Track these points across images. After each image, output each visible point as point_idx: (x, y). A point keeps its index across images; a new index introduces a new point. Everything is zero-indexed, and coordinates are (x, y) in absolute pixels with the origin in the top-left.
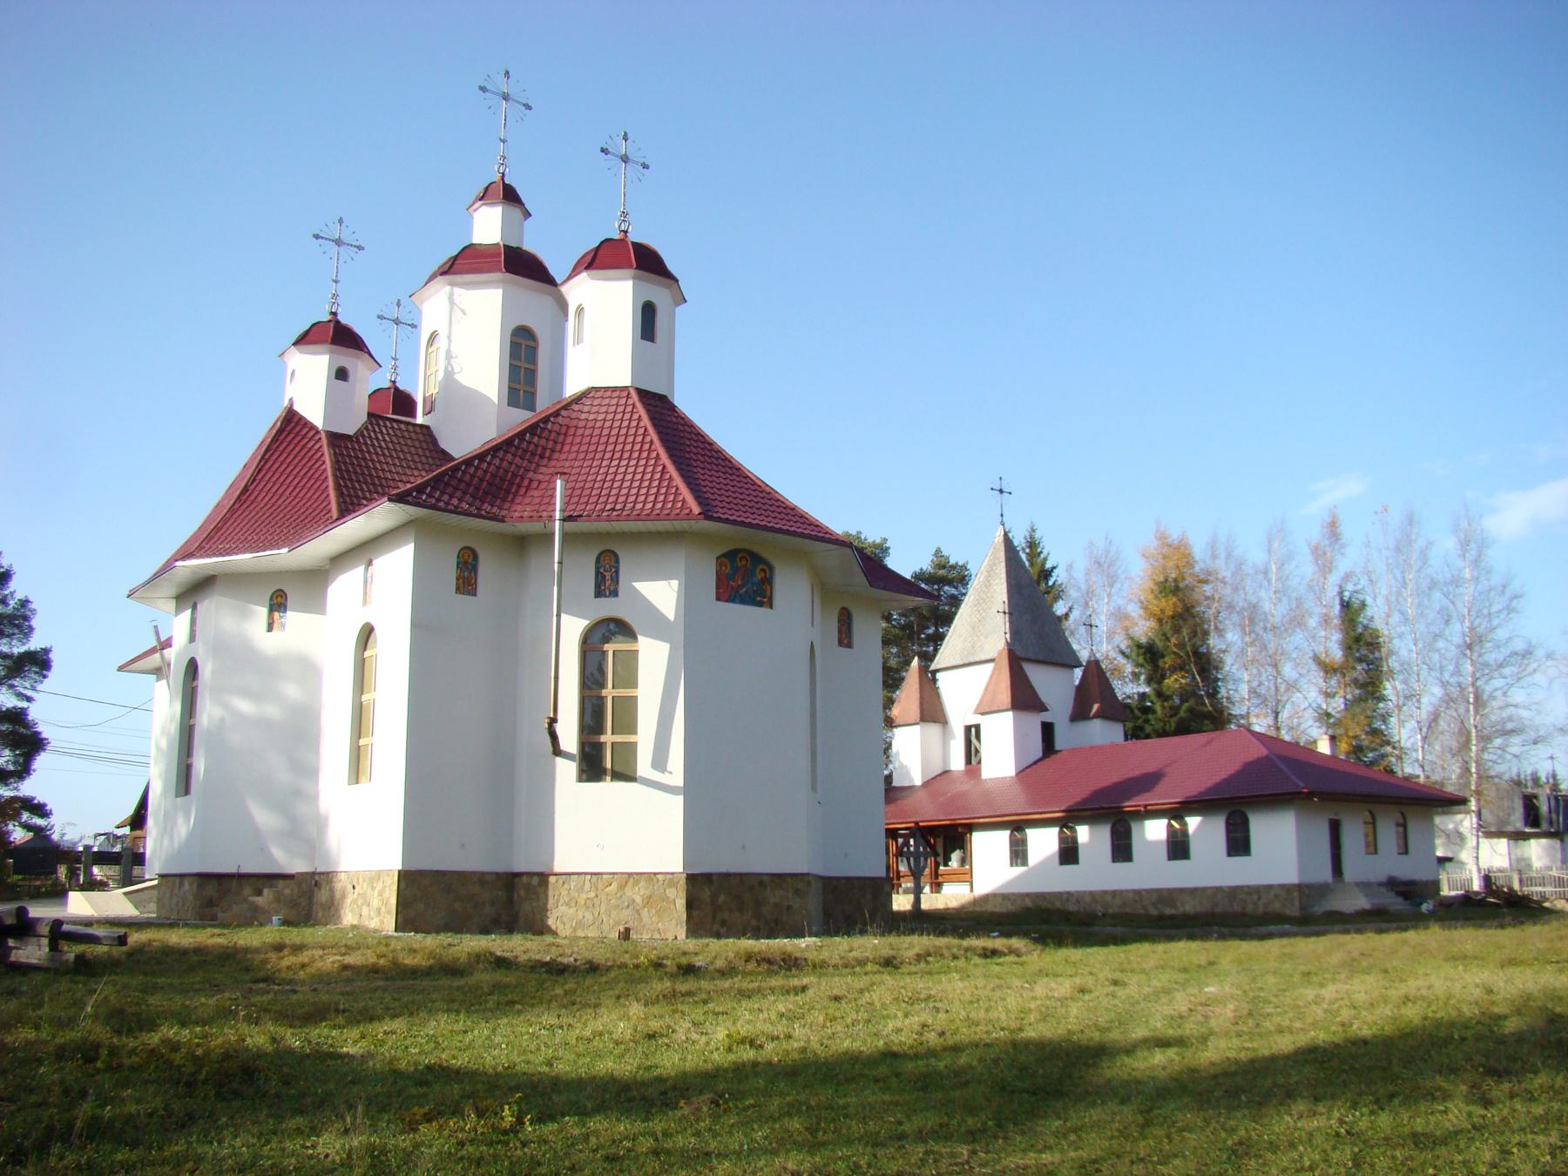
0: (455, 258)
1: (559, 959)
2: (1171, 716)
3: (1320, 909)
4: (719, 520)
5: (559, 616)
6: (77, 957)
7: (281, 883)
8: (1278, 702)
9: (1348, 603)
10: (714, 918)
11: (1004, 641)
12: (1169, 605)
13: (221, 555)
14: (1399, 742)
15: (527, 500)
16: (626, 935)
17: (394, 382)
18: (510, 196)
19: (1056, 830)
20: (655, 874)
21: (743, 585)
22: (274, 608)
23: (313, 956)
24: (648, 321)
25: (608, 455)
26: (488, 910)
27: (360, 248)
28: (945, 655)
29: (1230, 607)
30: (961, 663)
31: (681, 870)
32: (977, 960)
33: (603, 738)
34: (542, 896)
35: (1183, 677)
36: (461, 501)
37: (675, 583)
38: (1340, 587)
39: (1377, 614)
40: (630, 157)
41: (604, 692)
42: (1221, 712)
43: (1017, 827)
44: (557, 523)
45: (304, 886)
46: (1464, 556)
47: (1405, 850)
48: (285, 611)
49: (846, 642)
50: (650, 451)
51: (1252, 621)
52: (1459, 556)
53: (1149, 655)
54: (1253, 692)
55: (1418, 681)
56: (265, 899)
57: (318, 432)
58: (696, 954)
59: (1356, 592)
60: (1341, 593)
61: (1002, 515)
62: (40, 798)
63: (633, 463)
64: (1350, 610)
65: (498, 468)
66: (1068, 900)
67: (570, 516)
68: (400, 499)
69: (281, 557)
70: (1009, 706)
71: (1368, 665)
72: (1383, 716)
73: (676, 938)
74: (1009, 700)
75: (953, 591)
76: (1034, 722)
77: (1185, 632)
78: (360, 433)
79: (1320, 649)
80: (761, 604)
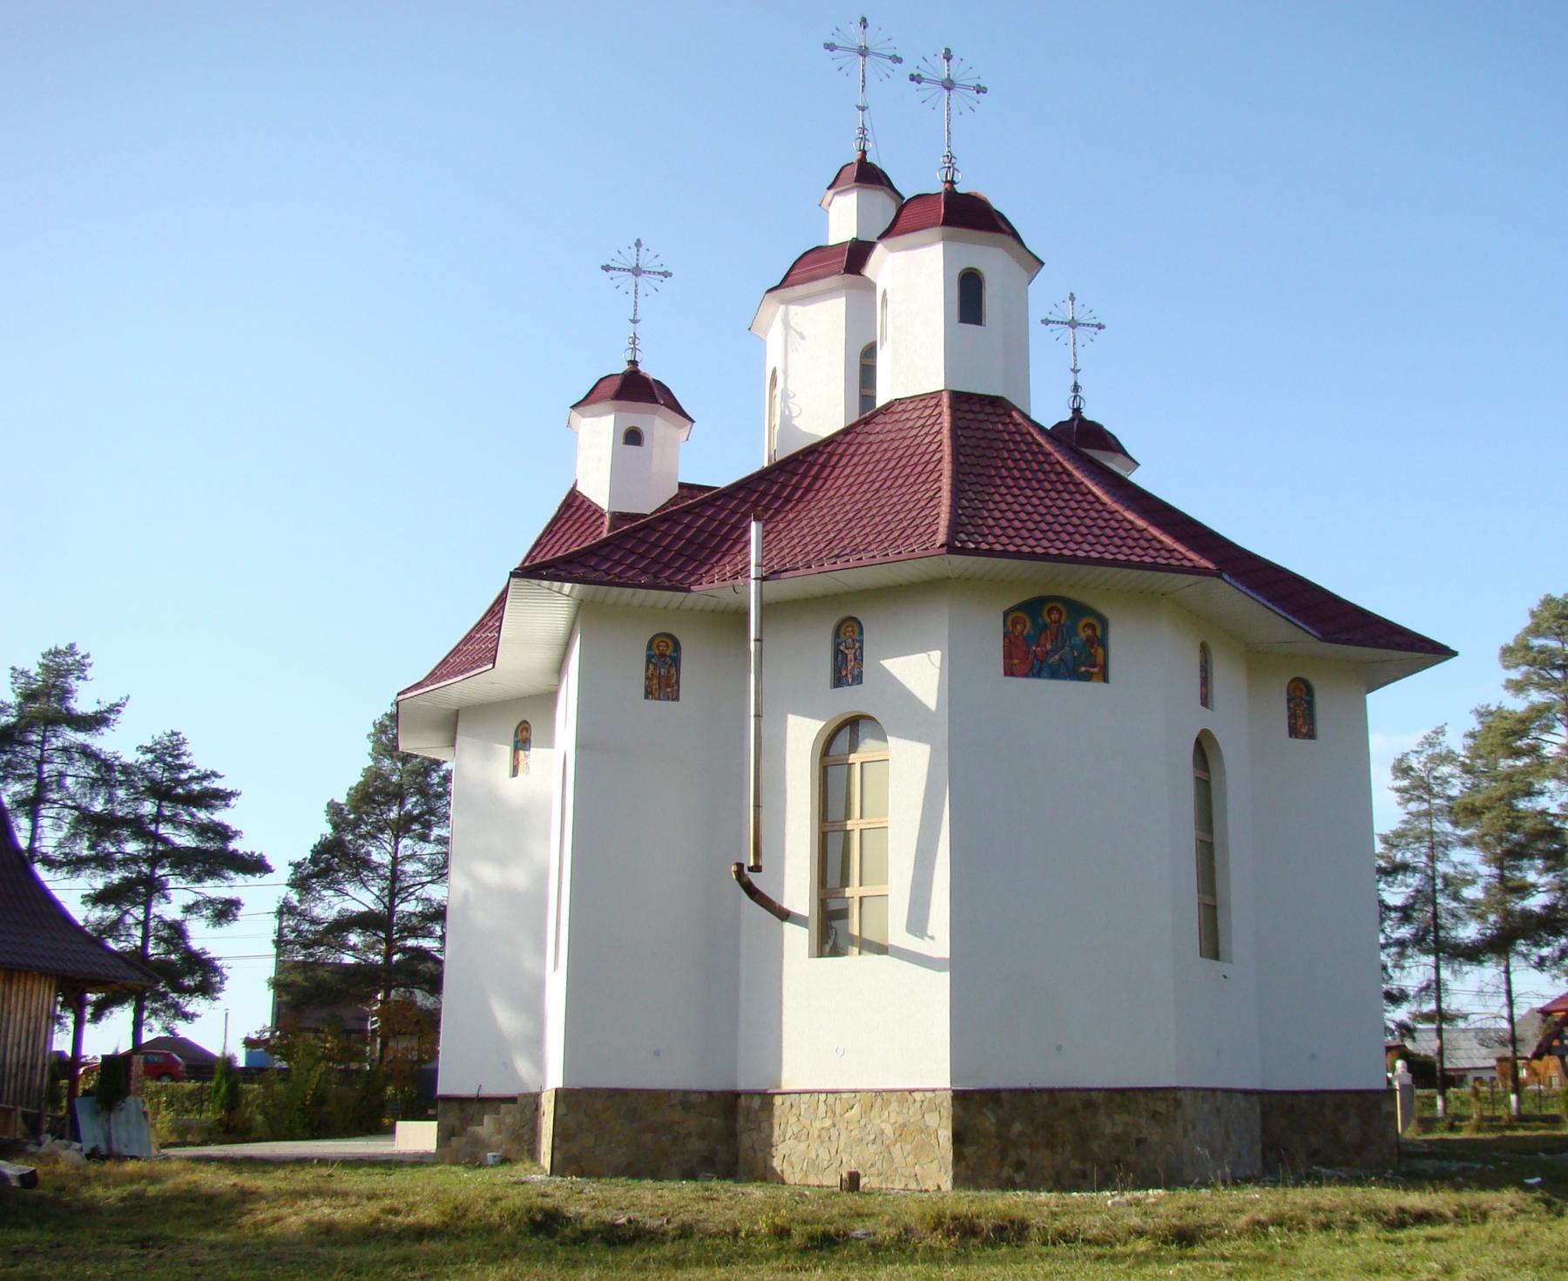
10: (1003, 1159)
16: (853, 1182)
20: (911, 1091)
21: (1054, 651)
22: (520, 745)
26: (696, 1145)
27: (666, 274)
31: (948, 1086)
34: (765, 1125)
37: (936, 655)
44: (753, 583)
48: (529, 750)
49: (1304, 730)
57: (602, 515)
73: (939, 1188)
80: (1087, 677)
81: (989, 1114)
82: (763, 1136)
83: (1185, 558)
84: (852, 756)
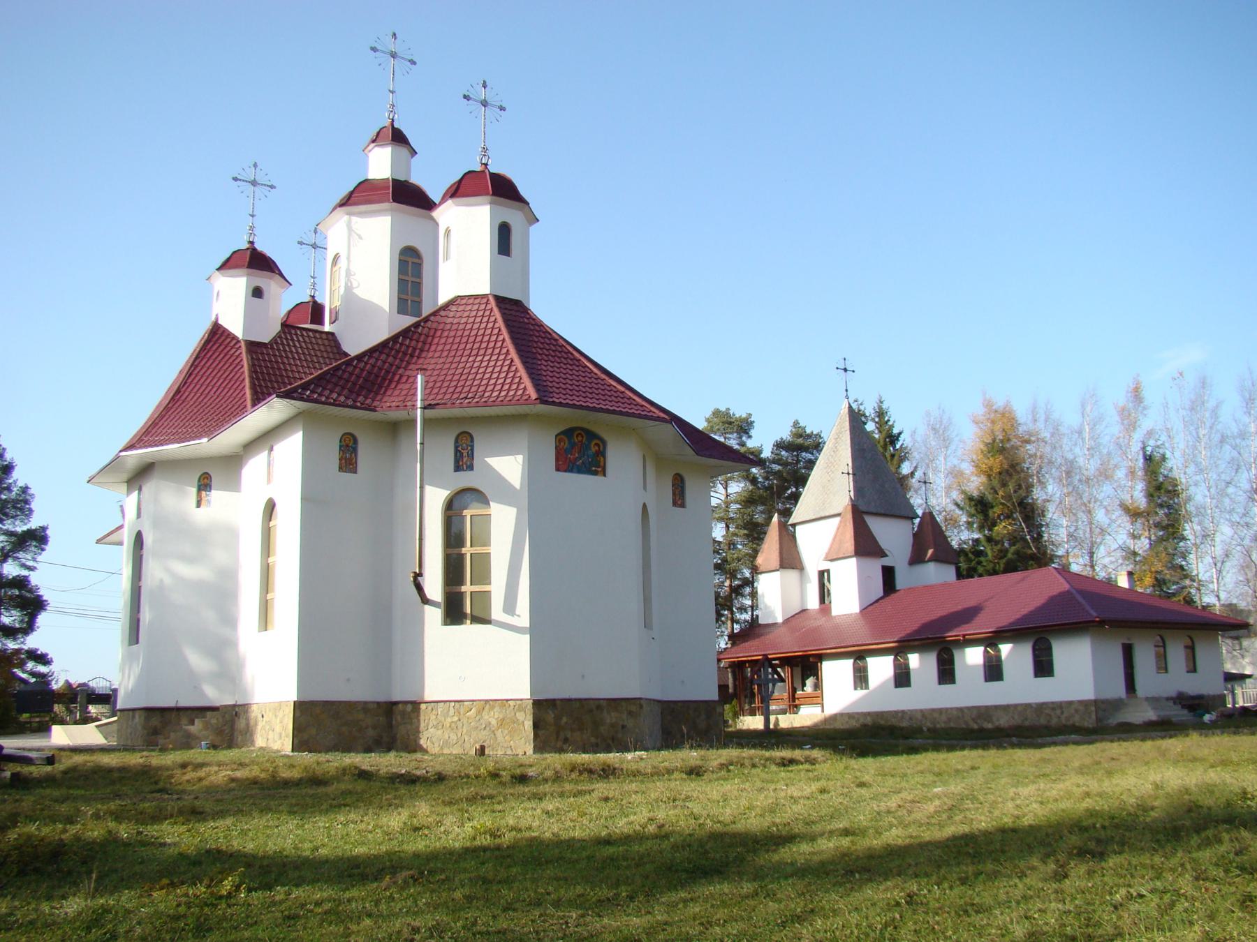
0: (352, 193)
1: (414, 772)
2: (1001, 558)
3: (1113, 721)
4: (553, 403)
5: (422, 487)
6: (13, 775)
7: (209, 714)
8: (1093, 543)
9: (1150, 456)
10: (557, 737)
11: (848, 498)
12: (997, 462)
13: (156, 446)
14: (1197, 575)
15: (397, 392)
17: (313, 297)
18: (399, 138)
19: (891, 658)
20: (507, 700)
23: (210, 771)
24: (504, 239)
25: (467, 353)
26: (371, 733)
27: (272, 187)
28: (799, 514)
29: (1050, 462)
30: (814, 517)
32: (774, 768)
33: (463, 589)
35: (1010, 524)
36: (339, 395)
37: (520, 458)
38: (1143, 443)
39: (1175, 465)
40: (489, 101)
41: (464, 550)
42: (1045, 553)
43: (860, 656)
44: (419, 410)
45: (227, 716)
46: (1249, 413)
47: (1193, 669)
48: (210, 491)
50: (501, 347)
51: (1068, 473)
52: (1245, 413)
53: (979, 507)
54: (1070, 535)
55: (1212, 522)
56: (197, 727)
57: (238, 341)
58: (531, 766)
59: (1158, 447)
60: (1144, 449)
61: (847, 390)
62: (42, 649)
63: (494, 358)
64: (1152, 463)
65: (374, 366)
66: (902, 717)
67: (430, 405)
68: (287, 395)
69: (203, 446)
70: (853, 553)
71: (1169, 509)
72: (1183, 553)
74: (853, 548)
75: (809, 456)
76: (875, 566)
77: (1011, 487)
78: (274, 340)
79: (1126, 498)
80: (595, 473)
81: (551, 712)
82: (414, 727)
83: (651, 411)
84: (465, 511)
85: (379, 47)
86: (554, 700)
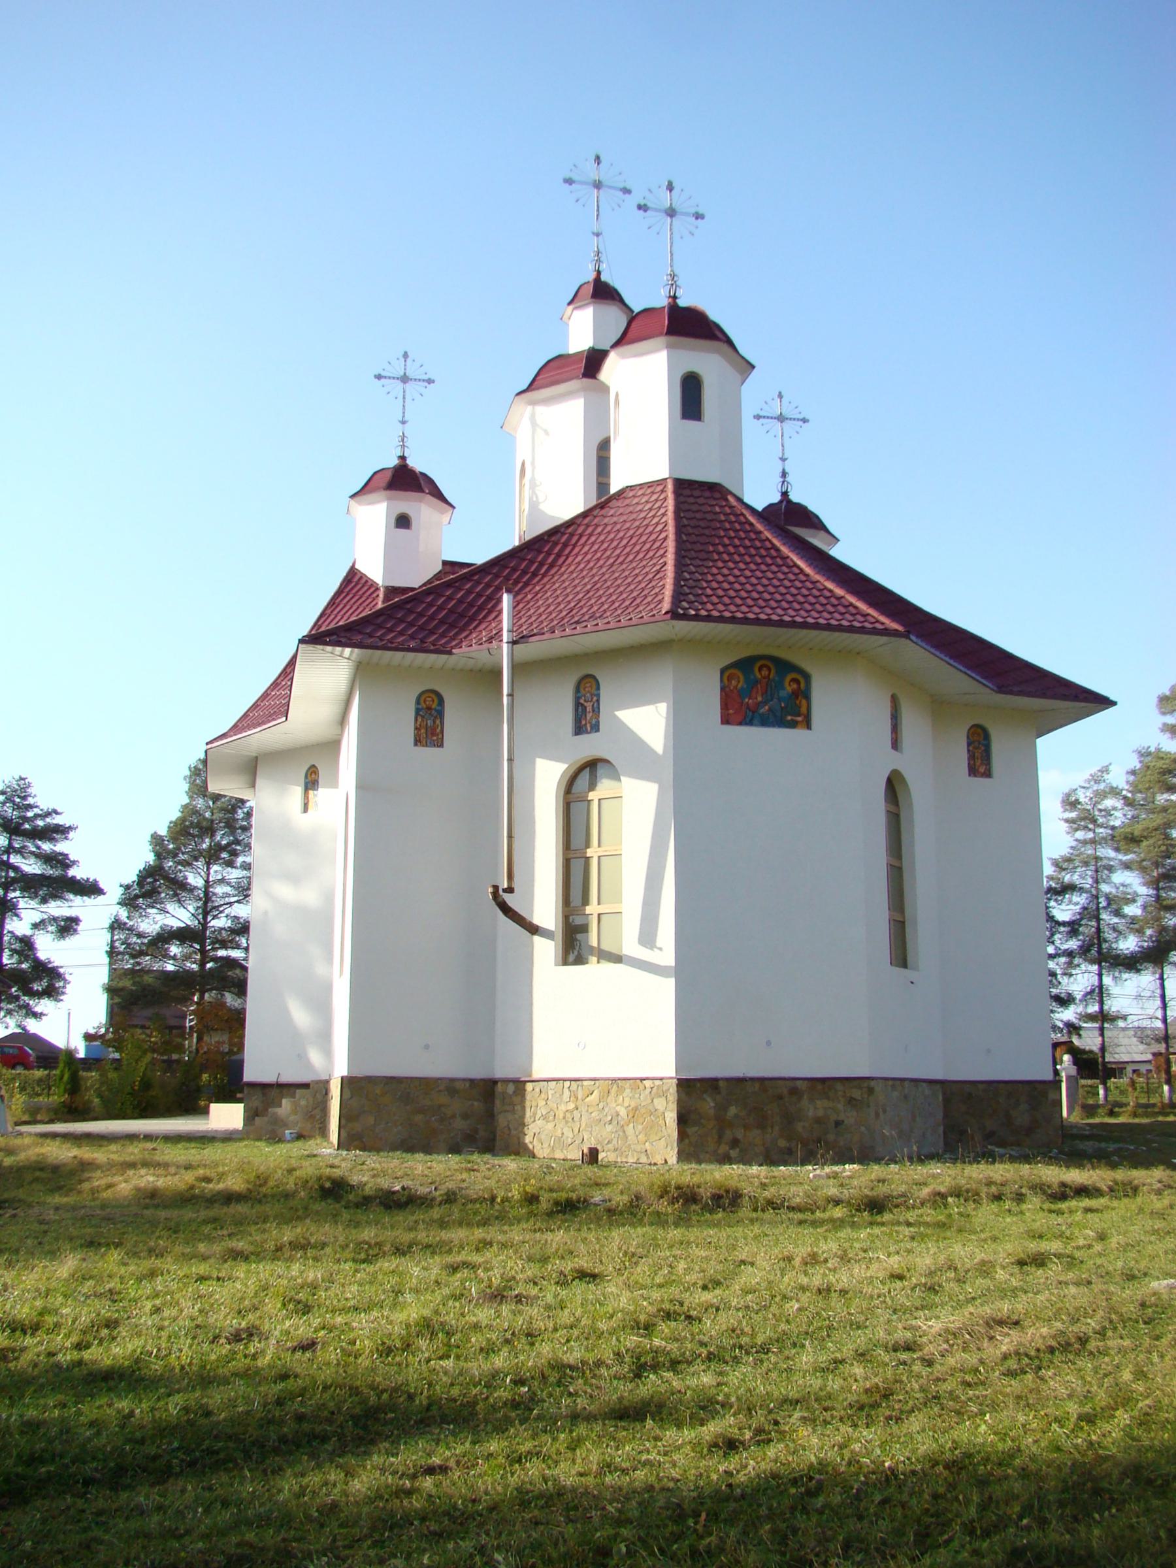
7: (299, 1092)
10: (720, 1137)
16: (592, 1156)
20: (642, 1080)
21: (765, 703)
26: (460, 1124)
27: (430, 381)
34: (518, 1108)
37: (663, 707)
40: (678, 210)
41: (589, 853)
44: (505, 647)
49: (982, 770)
57: (377, 589)
73: (666, 1162)
80: (793, 725)
81: (709, 1099)
83: (877, 621)
85: (575, 177)
86: (716, 1080)
